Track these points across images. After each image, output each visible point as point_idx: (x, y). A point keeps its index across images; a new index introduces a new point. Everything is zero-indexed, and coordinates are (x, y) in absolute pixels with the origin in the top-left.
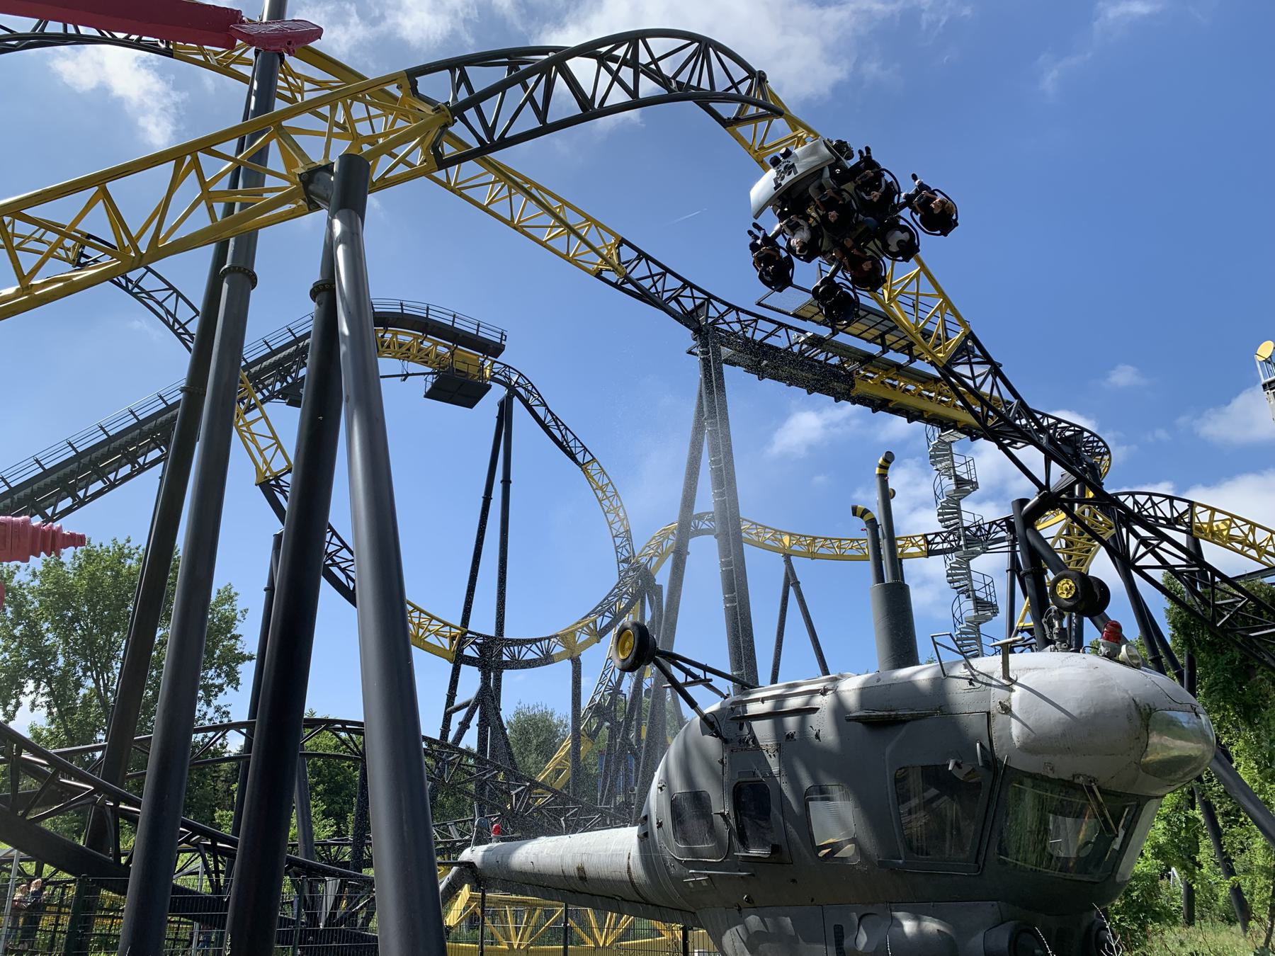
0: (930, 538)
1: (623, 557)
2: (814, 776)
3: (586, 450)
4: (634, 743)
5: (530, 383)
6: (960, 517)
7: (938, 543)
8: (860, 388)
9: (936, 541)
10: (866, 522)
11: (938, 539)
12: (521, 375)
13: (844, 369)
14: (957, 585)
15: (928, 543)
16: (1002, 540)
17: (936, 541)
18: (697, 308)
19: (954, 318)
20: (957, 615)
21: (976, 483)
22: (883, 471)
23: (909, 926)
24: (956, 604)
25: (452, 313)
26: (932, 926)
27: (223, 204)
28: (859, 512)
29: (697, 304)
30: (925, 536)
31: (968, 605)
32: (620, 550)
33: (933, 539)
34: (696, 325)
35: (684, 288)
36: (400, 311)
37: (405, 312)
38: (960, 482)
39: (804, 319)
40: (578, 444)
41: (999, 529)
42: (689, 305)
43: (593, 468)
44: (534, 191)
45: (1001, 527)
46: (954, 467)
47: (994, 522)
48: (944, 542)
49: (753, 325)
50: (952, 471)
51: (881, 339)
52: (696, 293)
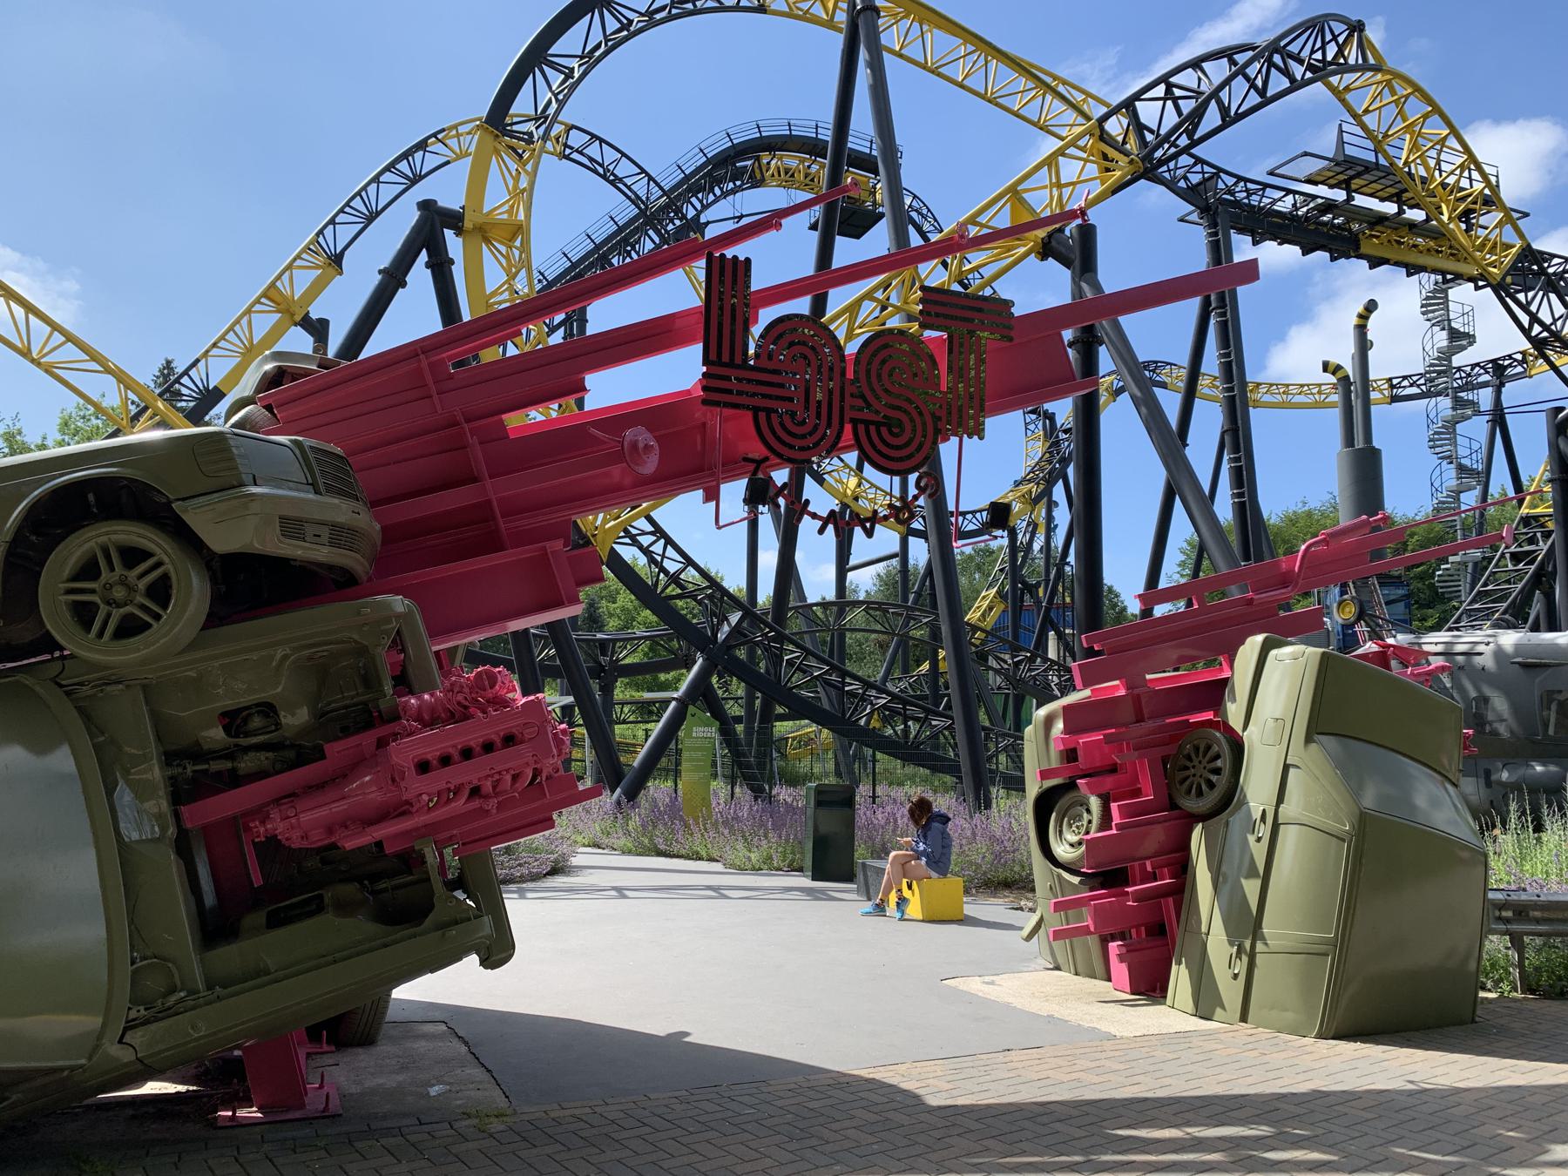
0: (1395, 382)
2: (1478, 689)
4: (996, 588)
5: (925, 205)
7: (1404, 387)
8: (1364, 250)
9: (1403, 384)
10: (1338, 380)
11: (1405, 383)
12: (915, 197)
13: (1350, 230)
14: (1438, 450)
15: (1392, 387)
16: (1485, 385)
17: (1403, 384)
18: (1205, 180)
19: (1487, 172)
20: (1437, 484)
21: (1474, 335)
22: (1362, 322)
23: (1539, 768)
24: (1437, 472)
26: (1553, 768)
28: (1331, 368)
30: (1390, 379)
31: (1450, 472)
33: (1400, 383)
34: (1203, 204)
35: (1195, 164)
37: (793, 133)
38: (1454, 335)
39: (1315, 183)
41: (1482, 371)
42: (1195, 179)
44: (1061, 88)
45: (1485, 369)
46: (1449, 320)
47: (1477, 365)
48: (1411, 385)
49: (1260, 193)
50: (1446, 323)
51: (1397, 198)
52: (1207, 168)
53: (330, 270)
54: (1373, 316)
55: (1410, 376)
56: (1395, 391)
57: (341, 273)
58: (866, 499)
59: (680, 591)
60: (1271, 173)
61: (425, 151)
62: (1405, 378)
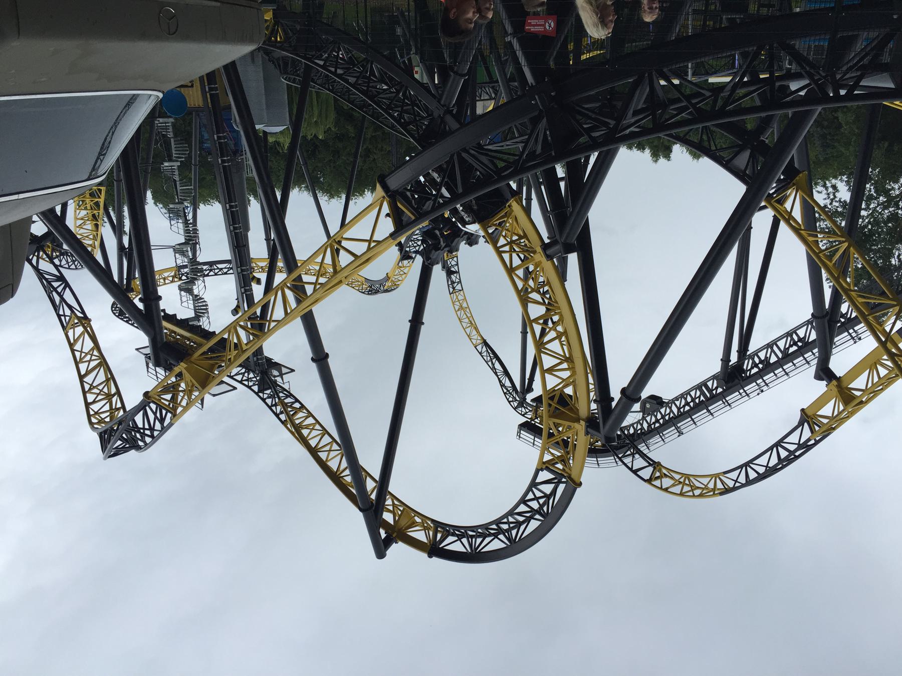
1: (455, 275)
3: (480, 353)
6: (195, 307)
7: (225, 268)
9: (226, 270)
11: (225, 270)
17: (226, 270)
25: (733, 405)
27: (299, 317)
29: (541, 503)
32: (457, 280)
33: (228, 271)
36: (599, 459)
40: (485, 358)
43: (477, 339)
48: (221, 269)
53: (810, 413)
54: (234, 306)
55: (223, 274)
56: (231, 266)
57: (803, 410)
58: (329, 273)
59: (251, 277)
60: (235, 388)
61: (767, 467)
62: (226, 273)
